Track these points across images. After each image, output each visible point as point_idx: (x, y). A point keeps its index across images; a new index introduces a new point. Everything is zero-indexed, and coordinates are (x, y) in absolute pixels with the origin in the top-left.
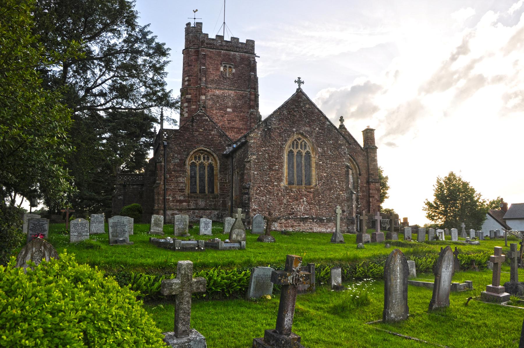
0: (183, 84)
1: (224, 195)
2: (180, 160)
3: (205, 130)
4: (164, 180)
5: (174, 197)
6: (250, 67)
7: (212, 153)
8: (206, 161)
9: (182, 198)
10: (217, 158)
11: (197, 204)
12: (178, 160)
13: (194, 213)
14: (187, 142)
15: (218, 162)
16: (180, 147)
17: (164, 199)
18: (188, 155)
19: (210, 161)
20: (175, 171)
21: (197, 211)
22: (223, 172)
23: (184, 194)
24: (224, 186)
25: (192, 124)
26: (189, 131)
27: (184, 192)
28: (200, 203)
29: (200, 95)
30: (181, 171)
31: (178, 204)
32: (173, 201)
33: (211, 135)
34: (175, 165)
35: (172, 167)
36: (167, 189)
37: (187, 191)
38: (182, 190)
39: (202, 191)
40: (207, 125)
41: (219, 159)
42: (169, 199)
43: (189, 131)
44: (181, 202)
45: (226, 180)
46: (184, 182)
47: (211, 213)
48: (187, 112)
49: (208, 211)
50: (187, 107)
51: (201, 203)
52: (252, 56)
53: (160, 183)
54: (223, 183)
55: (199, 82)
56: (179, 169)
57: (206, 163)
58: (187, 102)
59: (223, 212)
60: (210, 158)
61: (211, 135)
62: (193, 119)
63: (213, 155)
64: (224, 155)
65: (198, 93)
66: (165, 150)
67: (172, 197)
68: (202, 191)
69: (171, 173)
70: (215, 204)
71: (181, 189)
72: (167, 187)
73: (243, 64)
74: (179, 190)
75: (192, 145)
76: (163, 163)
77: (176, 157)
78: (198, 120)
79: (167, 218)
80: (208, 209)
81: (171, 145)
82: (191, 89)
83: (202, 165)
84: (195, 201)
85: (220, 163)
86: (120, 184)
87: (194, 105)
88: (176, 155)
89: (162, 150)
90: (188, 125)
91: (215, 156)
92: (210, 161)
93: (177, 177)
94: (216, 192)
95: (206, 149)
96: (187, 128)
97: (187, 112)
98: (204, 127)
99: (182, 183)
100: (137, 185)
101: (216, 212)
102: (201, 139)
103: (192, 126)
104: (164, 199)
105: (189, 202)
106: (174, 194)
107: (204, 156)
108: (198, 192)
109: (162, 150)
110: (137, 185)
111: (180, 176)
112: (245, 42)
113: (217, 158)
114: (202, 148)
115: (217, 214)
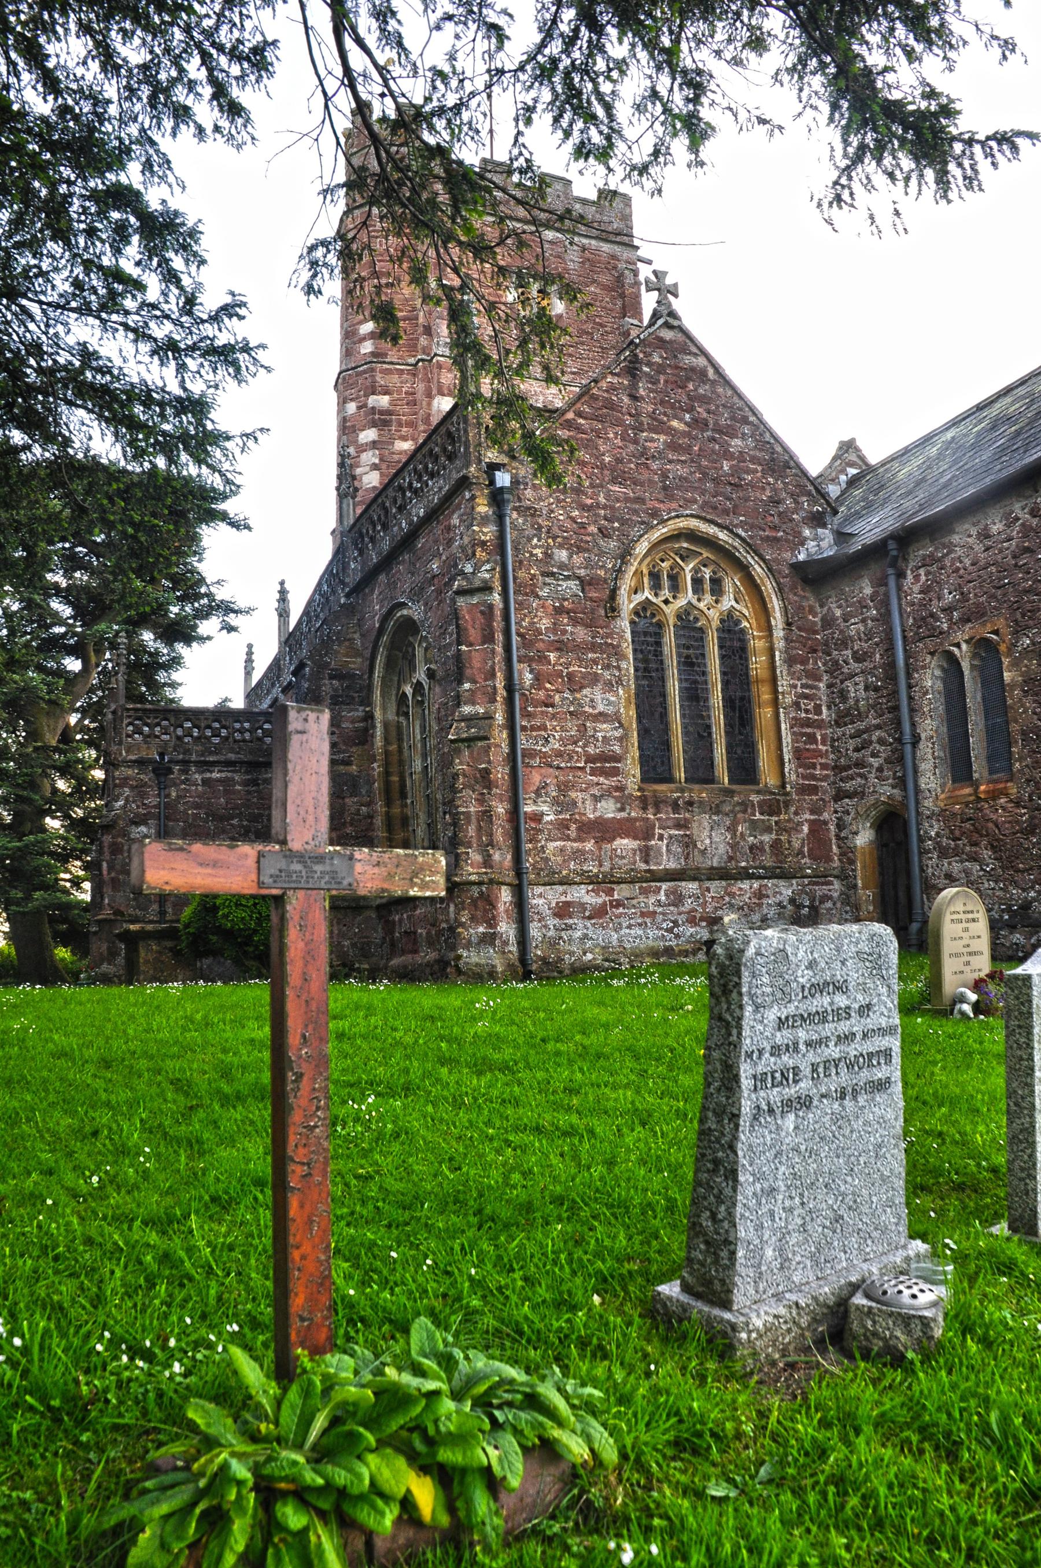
0: (348, 352)
1: (814, 790)
2: (583, 583)
3: (697, 423)
4: (510, 701)
5: (562, 804)
6: (622, 296)
7: (742, 553)
8: (708, 598)
9: (608, 809)
10: (768, 587)
11: (688, 843)
12: (573, 585)
13: (677, 899)
14: (614, 481)
15: (775, 604)
16: (583, 507)
17: (514, 812)
18: (625, 555)
19: (728, 602)
20: (560, 647)
21: (692, 887)
22: (804, 662)
23: (621, 789)
24: (812, 738)
25: (634, 386)
26: (620, 423)
27: (615, 772)
28: (704, 840)
29: (430, 396)
30: (593, 647)
31: (589, 845)
32: (563, 825)
33: (727, 455)
34: (559, 611)
35: (545, 623)
36: (529, 754)
37: (632, 771)
38: (605, 763)
39: (701, 771)
40: (704, 400)
41: (780, 590)
42: (537, 817)
43: (620, 423)
44: (603, 831)
45: (818, 710)
46: (616, 718)
47: (760, 895)
48: (375, 467)
49: (745, 885)
50: (374, 444)
51: (713, 839)
52: (626, 254)
53: (489, 717)
54: (807, 723)
55: (423, 341)
56: (581, 634)
57: (712, 612)
58: (374, 424)
59: (820, 890)
60: (728, 586)
61: (727, 455)
62: (634, 360)
63: (744, 570)
64: (798, 568)
65: (421, 387)
66: (500, 519)
67: (555, 802)
68: (701, 771)
69: (543, 659)
70: (776, 845)
71: (603, 758)
72: (523, 742)
73: (594, 281)
74: (590, 759)
75: (640, 500)
76: (496, 598)
77: (562, 566)
78: (660, 369)
79: (534, 931)
80: (745, 875)
81: (529, 493)
82: (388, 372)
83: (689, 626)
84: (678, 826)
85: (785, 610)
86: (140, 763)
87: (404, 439)
88: (562, 555)
89: (484, 520)
90: (612, 388)
91: (758, 570)
92: (728, 602)
93: (574, 684)
94: (769, 778)
95: (711, 530)
96: (611, 406)
97: (375, 467)
98: (691, 410)
99: (602, 717)
100: (228, 764)
101: (786, 890)
102: (682, 471)
103: (634, 398)
104: (514, 812)
105: (648, 835)
106: (564, 788)
107: (696, 570)
108: (681, 774)
109: (484, 520)
110: (228, 764)
111: (595, 679)
112: (593, 196)
113: (768, 587)
114: (694, 523)
115: (792, 901)
